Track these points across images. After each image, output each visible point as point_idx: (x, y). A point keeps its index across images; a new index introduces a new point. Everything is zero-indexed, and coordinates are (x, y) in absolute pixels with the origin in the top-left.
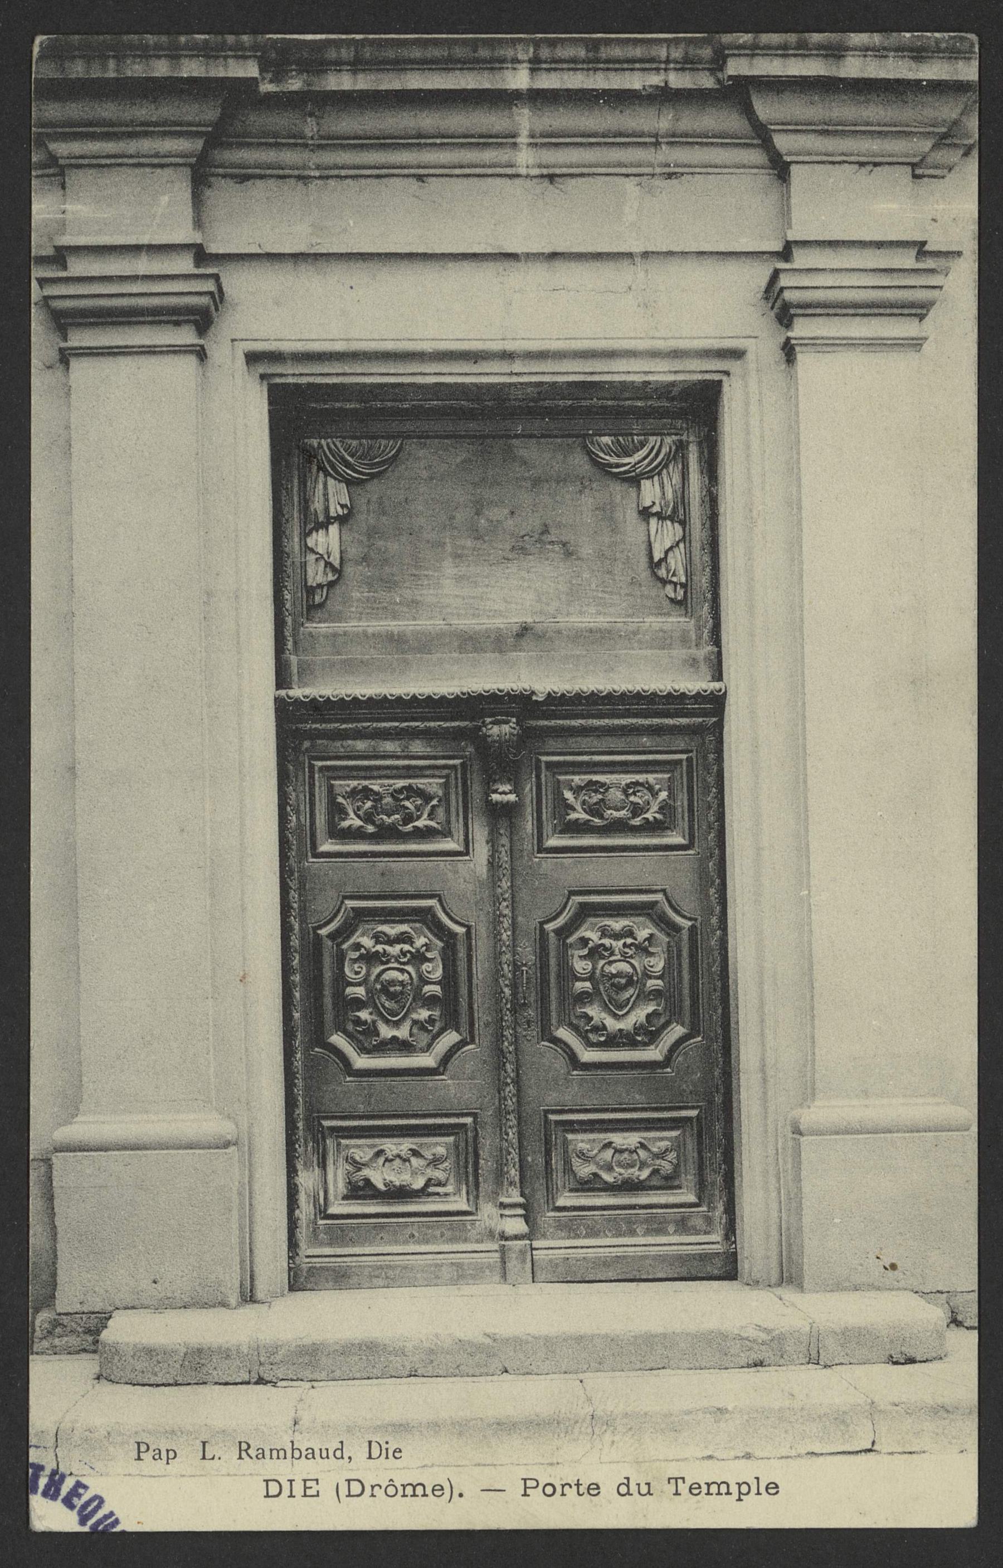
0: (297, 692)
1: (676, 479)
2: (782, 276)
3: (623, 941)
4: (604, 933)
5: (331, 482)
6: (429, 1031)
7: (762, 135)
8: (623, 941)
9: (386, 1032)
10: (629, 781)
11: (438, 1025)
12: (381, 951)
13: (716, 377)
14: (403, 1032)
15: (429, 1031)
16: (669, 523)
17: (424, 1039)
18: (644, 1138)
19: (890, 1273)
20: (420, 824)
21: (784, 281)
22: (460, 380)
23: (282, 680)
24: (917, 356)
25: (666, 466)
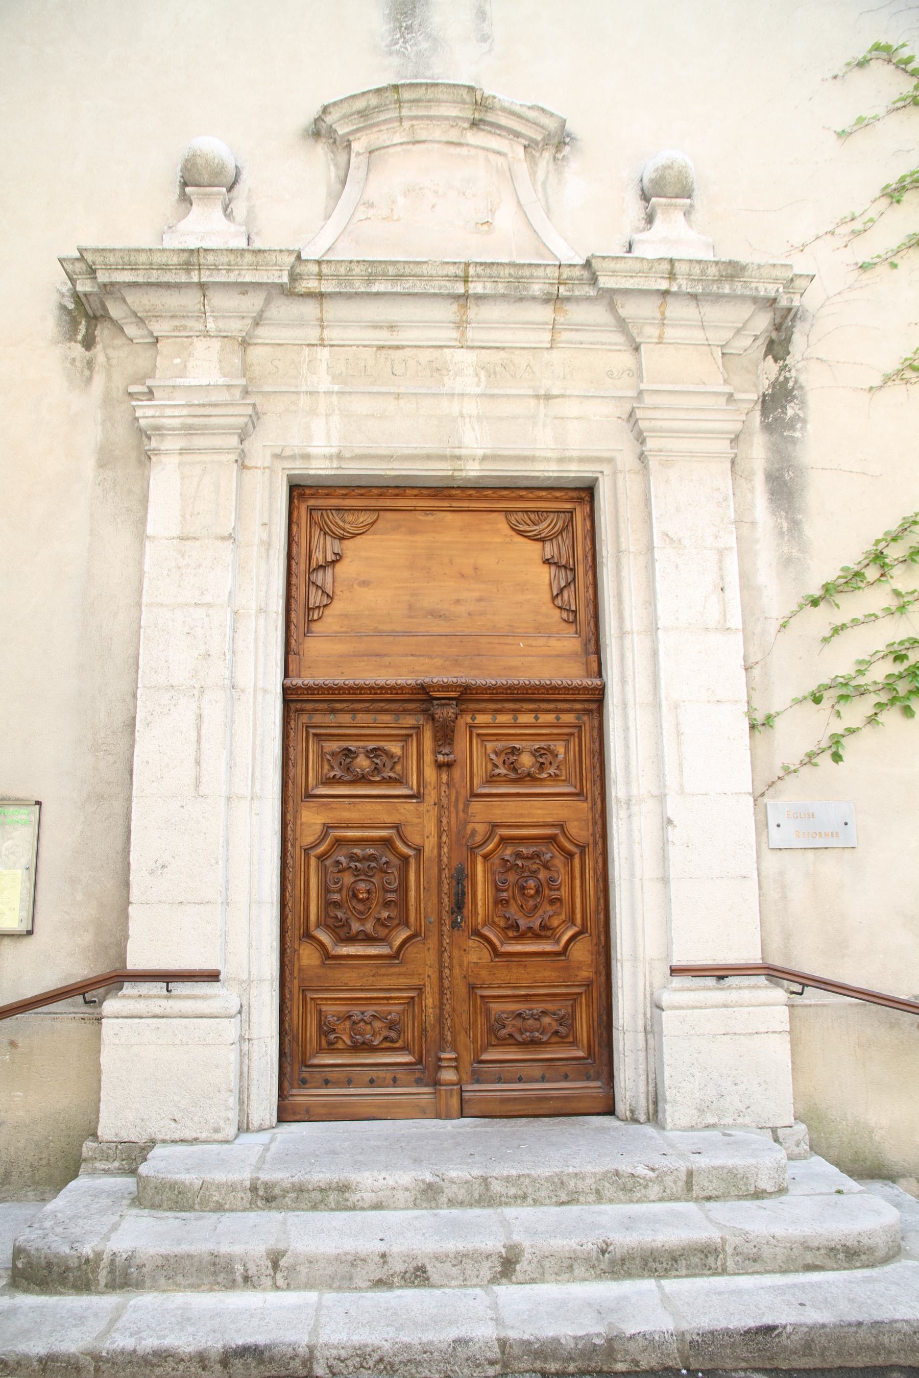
0: (296, 681)
1: (568, 542)
2: (137, 410)
3: (367, 864)
4: (519, 855)
5: (328, 538)
6: (387, 926)
7: (622, 325)
8: (367, 864)
9: (356, 927)
10: (537, 747)
11: (396, 922)
12: (354, 867)
13: (595, 475)
14: (369, 927)
15: (387, 926)
16: (563, 571)
17: (382, 932)
18: (376, 1011)
19: (172, 1123)
20: (385, 775)
21: (139, 413)
22: (382, 473)
23: (286, 675)
24: (299, 468)
25: (561, 532)
